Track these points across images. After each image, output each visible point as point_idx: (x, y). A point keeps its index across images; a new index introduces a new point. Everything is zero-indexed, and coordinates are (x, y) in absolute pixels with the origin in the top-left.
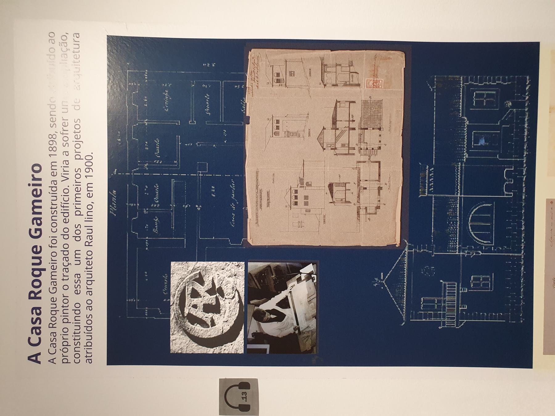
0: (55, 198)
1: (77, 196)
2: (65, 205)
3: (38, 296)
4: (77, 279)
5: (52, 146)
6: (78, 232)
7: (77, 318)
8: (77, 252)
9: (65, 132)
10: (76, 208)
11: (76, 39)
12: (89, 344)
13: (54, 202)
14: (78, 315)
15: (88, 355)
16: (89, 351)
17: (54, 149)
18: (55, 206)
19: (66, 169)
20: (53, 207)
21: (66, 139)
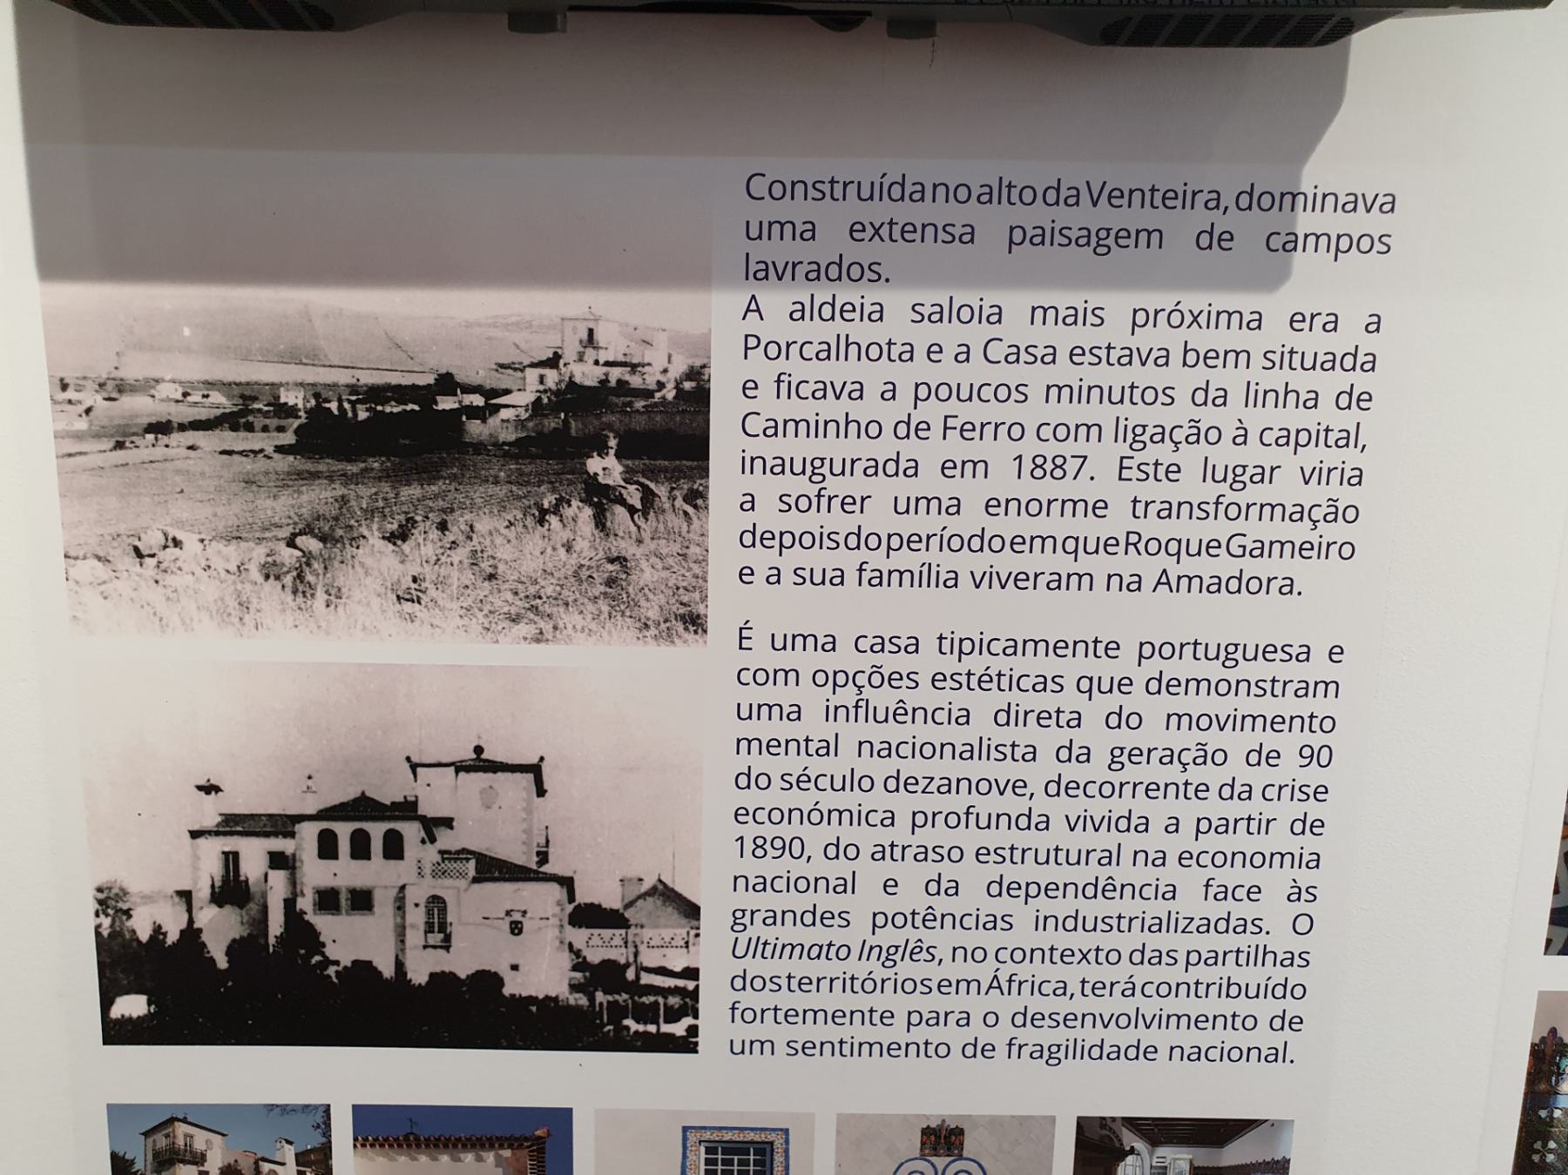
0: (865, 194)
2: (862, 712)
3: (1131, 548)
4: (957, 231)
8: (792, 675)
9: (824, 501)
11: (1275, 585)
12: (1234, 990)
15: (898, 852)
16: (1214, 990)
18: (1017, 858)
19: (1335, 475)
20: (838, 189)
21: (803, 504)
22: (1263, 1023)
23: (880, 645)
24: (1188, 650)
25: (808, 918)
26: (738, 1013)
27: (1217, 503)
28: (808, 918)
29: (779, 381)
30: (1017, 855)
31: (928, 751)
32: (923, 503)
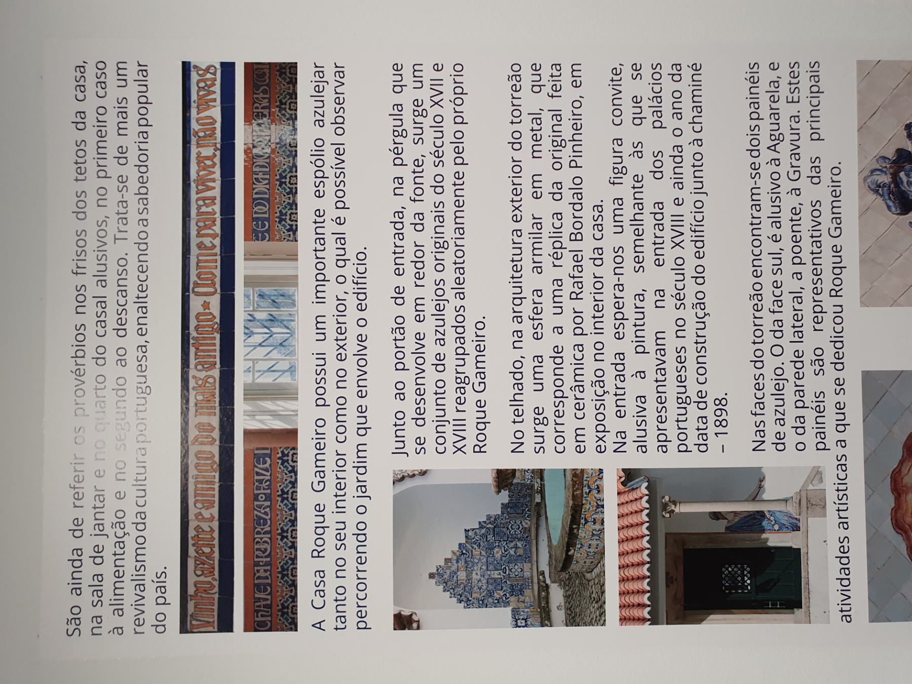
1: (535, 148)
2: (698, 228)
5: (720, 419)
6: (460, 319)
7: (819, 420)
10: (140, 150)
13: (700, 333)
14: (559, 366)
17: (724, 423)
18: (702, 340)
20: (700, 340)
22: (677, 86)
23: (81, 88)
24: (681, 425)
25: (558, 361)
26: (417, 198)
27: (533, 319)
28: (558, 361)
29: (614, 183)
30: (700, 340)
31: (341, 308)
32: (319, 326)
